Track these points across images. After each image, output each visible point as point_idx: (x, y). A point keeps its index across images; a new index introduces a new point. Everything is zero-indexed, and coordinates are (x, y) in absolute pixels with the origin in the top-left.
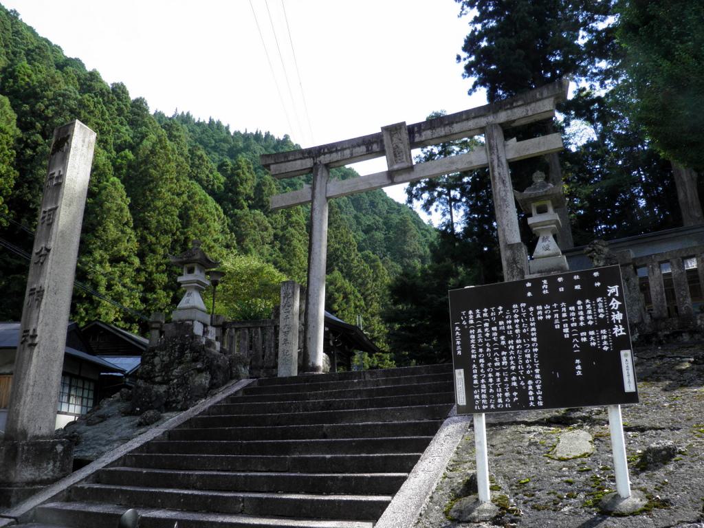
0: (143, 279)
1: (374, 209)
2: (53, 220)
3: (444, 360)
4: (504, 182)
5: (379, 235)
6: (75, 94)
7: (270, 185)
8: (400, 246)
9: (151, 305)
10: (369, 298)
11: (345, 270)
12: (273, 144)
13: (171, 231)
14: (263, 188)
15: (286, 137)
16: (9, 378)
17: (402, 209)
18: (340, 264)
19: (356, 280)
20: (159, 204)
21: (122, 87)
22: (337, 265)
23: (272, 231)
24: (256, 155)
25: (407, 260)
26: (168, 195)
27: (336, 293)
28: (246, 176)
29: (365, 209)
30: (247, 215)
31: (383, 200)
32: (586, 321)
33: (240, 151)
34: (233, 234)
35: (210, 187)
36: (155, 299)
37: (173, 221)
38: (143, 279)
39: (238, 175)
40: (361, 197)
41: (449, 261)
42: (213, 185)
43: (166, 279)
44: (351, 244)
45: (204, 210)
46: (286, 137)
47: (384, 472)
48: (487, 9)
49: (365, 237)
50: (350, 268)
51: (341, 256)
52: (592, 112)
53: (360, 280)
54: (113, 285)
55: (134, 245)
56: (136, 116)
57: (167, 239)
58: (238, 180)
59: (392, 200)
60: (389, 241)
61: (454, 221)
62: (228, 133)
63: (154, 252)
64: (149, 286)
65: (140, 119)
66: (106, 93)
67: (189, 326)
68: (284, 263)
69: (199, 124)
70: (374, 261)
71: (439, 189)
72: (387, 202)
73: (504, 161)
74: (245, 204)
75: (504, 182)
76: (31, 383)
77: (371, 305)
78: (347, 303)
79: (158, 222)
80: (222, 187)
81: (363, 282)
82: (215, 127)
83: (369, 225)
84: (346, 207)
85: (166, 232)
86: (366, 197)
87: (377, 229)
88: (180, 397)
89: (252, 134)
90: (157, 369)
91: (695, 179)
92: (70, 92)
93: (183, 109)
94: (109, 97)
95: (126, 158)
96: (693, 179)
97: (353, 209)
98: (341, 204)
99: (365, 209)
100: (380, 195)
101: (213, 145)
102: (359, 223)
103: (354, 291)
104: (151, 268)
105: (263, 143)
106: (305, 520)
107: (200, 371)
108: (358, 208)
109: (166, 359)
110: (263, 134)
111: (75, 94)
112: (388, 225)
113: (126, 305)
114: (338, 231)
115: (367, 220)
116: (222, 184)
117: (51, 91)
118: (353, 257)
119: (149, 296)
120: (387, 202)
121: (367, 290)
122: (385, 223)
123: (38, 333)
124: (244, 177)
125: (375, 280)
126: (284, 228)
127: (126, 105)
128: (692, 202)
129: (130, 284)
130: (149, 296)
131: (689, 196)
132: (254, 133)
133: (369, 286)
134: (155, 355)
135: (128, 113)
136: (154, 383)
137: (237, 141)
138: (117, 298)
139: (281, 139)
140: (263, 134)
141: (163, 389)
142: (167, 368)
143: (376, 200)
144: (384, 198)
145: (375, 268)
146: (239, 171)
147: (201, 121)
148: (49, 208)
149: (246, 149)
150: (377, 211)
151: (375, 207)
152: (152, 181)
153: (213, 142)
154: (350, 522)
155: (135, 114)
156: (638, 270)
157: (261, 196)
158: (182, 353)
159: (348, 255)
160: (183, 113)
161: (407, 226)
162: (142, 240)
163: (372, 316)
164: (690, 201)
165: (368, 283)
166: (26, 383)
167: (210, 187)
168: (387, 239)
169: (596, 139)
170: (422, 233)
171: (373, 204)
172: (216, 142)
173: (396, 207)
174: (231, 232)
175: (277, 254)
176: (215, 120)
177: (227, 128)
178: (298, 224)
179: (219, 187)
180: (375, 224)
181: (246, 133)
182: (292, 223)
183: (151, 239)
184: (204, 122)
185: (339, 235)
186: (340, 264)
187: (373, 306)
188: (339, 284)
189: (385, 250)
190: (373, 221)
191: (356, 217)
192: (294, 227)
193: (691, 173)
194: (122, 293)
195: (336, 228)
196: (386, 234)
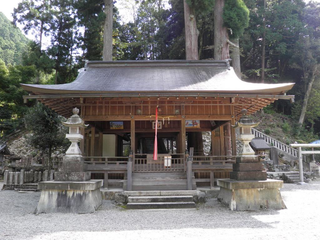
3: (19, 130)
5: (11, 52)
29: (6, 37)
31: (18, 35)
32: (258, 136)
40: (5, 29)
41: (33, 66)
60: (16, 56)
61: (42, 42)
72: (21, 36)
83: (6, 45)
86: (9, 30)
87: (11, 48)
91: (198, 35)
96: (196, 34)
99: (6, 37)
122: (16, 46)
128: (194, 49)
131: (192, 45)
144: (20, 34)
150: (14, 39)
151: (13, 37)
156: (53, 168)
164: (193, 48)
169: (133, 22)
173: (26, 40)
180: (10, 45)
193: (196, 30)
196: (16, 52)
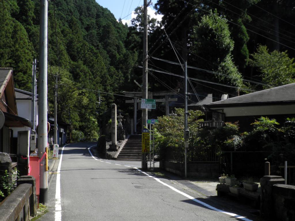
1: (89, 12)
5: (94, 31)
27: (81, 73)
28: (31, 6)
31: (94, 6)
39: (27, 5)
48: (140, 11)
49: (87, 33)
52: (141, 119)
58: (28, 8)
71: (124, 67)
78: (86, 77)
83: (88, 25)
84: (74, 12)
98: (72, 10)
102: (83, 23)
103: (88, 71)
106: (167, 179)
120: (96, 8)
124: (30, 7)
144: (95, 5)
151: (90, 11)
154: (200, 197)
161: (110, 28)
163: (97, 83)
170: (117, 31)
174: (31, 41)
188: (81, 68)
195: (75, 33)
196: (97, 31)
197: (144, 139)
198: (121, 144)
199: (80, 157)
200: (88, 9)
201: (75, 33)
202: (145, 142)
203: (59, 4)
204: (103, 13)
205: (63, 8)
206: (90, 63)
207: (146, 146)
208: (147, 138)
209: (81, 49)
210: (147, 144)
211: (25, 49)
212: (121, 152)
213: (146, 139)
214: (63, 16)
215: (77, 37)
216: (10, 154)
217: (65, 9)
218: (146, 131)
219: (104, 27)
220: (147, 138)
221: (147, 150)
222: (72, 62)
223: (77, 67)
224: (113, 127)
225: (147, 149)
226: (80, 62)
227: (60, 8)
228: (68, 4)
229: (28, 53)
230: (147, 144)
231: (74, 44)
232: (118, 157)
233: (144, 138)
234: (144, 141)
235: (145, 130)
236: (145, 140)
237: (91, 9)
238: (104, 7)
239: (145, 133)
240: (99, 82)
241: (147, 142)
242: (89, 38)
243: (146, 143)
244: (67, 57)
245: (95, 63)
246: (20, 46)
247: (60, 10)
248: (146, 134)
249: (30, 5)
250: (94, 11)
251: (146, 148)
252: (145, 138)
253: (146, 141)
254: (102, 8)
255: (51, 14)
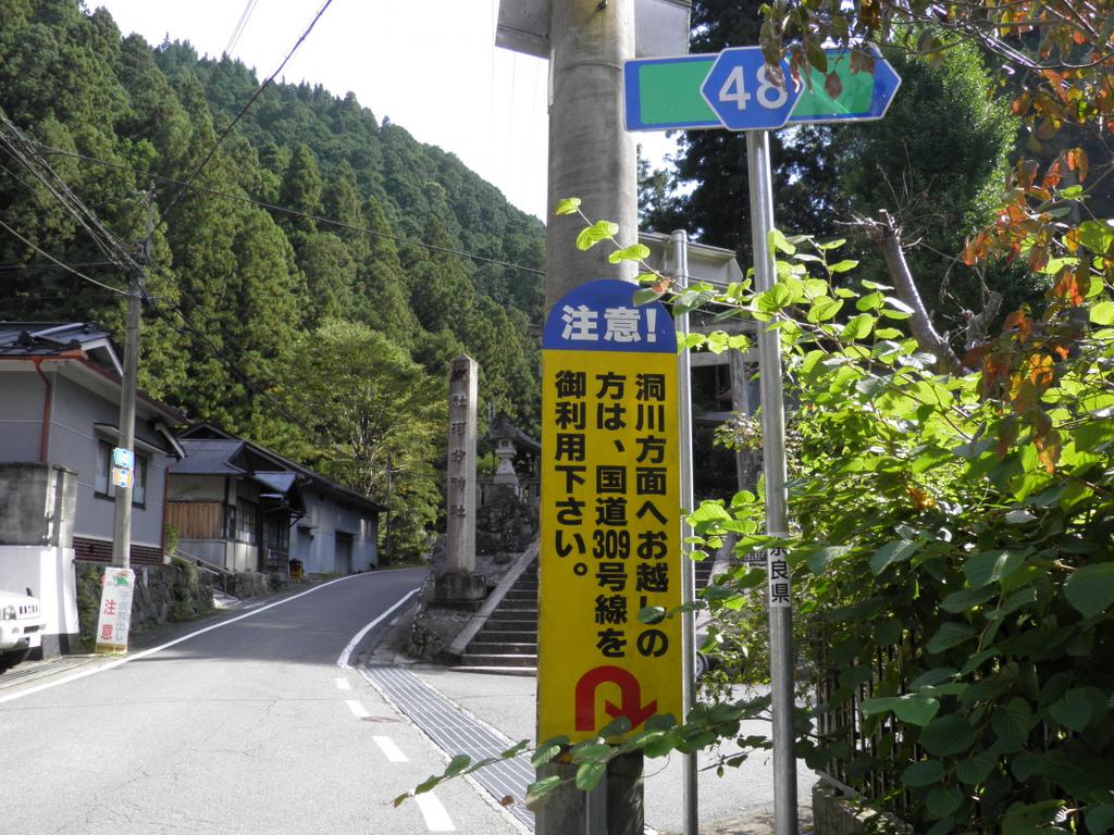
0: (189, 343)
2: (464, 432)
4: (741, 382)
5: (498, 267)
6: (50, 38)
7: (349, 194)
8: (528, 286)
9: (202, 379)
10: (490, 368)
11: (456, 327)
12: (327, 107)
13: (225, 272)
14: (339, 198)
15: (351, 95)
16: (199, 507)
17: (530, 224)
18: (449, 317)
19: (473, 341)
20: (207, 231)
21: (105, 16)
22: (445, 319)
23: (352, 265)
24: (302, 124)
25: (538, 307)
26: (217, 218)
30: (321, 244)
31: (500, 209)
33: (277, 115)
34: (303, 272)
35: (258, 193)
36: (206, 372)
37: (227, 260)
38: (189, 343)
39: (302, 177)
42: (262, 190)
43: (221, 343)
44: (465, 288)
45: (268, 241)
46: (351, 95)
47: (197, 636)
49: (476, 269)
50: (463, 323)
51: (451, 305)
53: (478, 342)
54: (151, 351)
55: (174, 294)
56: (131, 68)
57: (219, 284)
59: (515, 208)
62: (255, 82)
63: (200, 302)
64: (197, 353)
65: (138, 72)
66: (89, 33)
67: (510, 489)
68: (375, 316)
69: (205, 63)
70: (498, 313)
72: (506, 212)
73: (741, 363)
74: (313, 223)
75: (741, 382)
76: (465, 539)
77: (493, 379)
79: (205, 258)
80: (276, 193)
81: (483, 345)
82: (233, 70)
84: (447, 219)
85: (217, 274)
88: (516, 543)
89: (293, 86)
90: (493, 522)
92: (42, 35)
93: (178, 35)
94: (94, 39)
95: (146, 153)
97: (455, 222)
100: (497, 199)
101: (233, 103)
102: (467, 247)
104: (200, 326)
105: (312, 103)
107: (526, 523)
108: (465, 222)
109: (500, 514)
110: (312, 88)
111: (50, 38)
112: (511, 253)
113: (169, 380)
114: (443, 265)
115: (480, 241)
116: (275, 188)
117: (9, 30)
118: (468, 307)
119: (199, 366)
120: (506, 212)
121: (489, 357)
122: (506, 248)
123: (465, 508)
124: (312, 182)
125: (498, 342)
126: (368, 261)
127: (113, 48)
129: (170, 350)
130: (199, 366)
132: (298, 85)
133: (491, 351)
134: (490, 511)
135: (117, 60)
136: (491, 532)
137: (272, 99)
138: (156, 371)
139: (342, 99)
140: (312, 88)
141: (498, 536)
142: (501, 521)
143: (490, 209)
144: (502, 205)
145: (498, 323)
146: (302, 171)
147: (209, 59)
148: (458, 422)
149: (287, 112)
152: (194, 195)
153: (233, 98)
155: (127, 62)
157: (335, 211)
158: (513, 509)
159: (462, 305)
160: (177, 41)
162: (185, 284)
165: (489, 347)
166: (460, 539)
167: (258, 193)
168: (509, 273)
171: (486, 215)
172: (237, 98)
174: (300, 269)
175: (365, 305)
176: (233, 58)
177: (252, 73)
178: (390, 255)
179: (271, 194)
181: (283, 84)
182: (381, 253)
183: (197, 283)
184: (215, 60)
185: (446, 270)
186: (449, 317)
187: (496, 381)
188: (450, 350)
189: (507, 291)
190: (487, 243)
191: (462, 237)
192: (383, 260)
194: (162, 363)
195: (440, 259)
197: (572, 476)
198: (503, 574)
199: (122, 661)
200: (485, 215)
201: (440, 259)
202: (589, 515)
203: (408, 199)
204: (524, 227)
205: (418, 210)
206: (478, 337)
207: (610, 610)
208: (629, 459)
209: (452, 300)
210: (632, 564)
211: (274, 283)
212: (494, 615)
213: (611, 477)
214: (415, 228)
215: (446, 270)
216: (472, 589)
217: (422, 210)
218: (613, 314)
219: (524, 255)
220: (629, 459)
221: (628, 683)
222: (424, 334)
223: (439, 347)
224: (454, 480)
225: (632, 661)
226: (447, 333)
227: (408, 209)
228: (431, 203)
229: (282, 295)
230: (632, 564)
231: (433, 286)
232: (469, 649)
233: (572, 446)
234: (571, 509)
235: (584, 312)
236: (587, 492)
237: (493, 215)
238: (527, 213)
239: (593, 365)
240: (503, 392)
241: (636, 527)
242: (486, 283)
243: (612, 544)
244: (407, 315)
245: (492, 337)
246: (259, 272)
247: (408, 213)
248: (608, 379)
249: (311, 176)
250: (500, 220)
251: (610, 643)
252: (600, 448)
253: (613, 512)
254: (522, 214)
255: (371, 206)
